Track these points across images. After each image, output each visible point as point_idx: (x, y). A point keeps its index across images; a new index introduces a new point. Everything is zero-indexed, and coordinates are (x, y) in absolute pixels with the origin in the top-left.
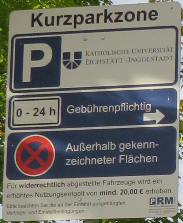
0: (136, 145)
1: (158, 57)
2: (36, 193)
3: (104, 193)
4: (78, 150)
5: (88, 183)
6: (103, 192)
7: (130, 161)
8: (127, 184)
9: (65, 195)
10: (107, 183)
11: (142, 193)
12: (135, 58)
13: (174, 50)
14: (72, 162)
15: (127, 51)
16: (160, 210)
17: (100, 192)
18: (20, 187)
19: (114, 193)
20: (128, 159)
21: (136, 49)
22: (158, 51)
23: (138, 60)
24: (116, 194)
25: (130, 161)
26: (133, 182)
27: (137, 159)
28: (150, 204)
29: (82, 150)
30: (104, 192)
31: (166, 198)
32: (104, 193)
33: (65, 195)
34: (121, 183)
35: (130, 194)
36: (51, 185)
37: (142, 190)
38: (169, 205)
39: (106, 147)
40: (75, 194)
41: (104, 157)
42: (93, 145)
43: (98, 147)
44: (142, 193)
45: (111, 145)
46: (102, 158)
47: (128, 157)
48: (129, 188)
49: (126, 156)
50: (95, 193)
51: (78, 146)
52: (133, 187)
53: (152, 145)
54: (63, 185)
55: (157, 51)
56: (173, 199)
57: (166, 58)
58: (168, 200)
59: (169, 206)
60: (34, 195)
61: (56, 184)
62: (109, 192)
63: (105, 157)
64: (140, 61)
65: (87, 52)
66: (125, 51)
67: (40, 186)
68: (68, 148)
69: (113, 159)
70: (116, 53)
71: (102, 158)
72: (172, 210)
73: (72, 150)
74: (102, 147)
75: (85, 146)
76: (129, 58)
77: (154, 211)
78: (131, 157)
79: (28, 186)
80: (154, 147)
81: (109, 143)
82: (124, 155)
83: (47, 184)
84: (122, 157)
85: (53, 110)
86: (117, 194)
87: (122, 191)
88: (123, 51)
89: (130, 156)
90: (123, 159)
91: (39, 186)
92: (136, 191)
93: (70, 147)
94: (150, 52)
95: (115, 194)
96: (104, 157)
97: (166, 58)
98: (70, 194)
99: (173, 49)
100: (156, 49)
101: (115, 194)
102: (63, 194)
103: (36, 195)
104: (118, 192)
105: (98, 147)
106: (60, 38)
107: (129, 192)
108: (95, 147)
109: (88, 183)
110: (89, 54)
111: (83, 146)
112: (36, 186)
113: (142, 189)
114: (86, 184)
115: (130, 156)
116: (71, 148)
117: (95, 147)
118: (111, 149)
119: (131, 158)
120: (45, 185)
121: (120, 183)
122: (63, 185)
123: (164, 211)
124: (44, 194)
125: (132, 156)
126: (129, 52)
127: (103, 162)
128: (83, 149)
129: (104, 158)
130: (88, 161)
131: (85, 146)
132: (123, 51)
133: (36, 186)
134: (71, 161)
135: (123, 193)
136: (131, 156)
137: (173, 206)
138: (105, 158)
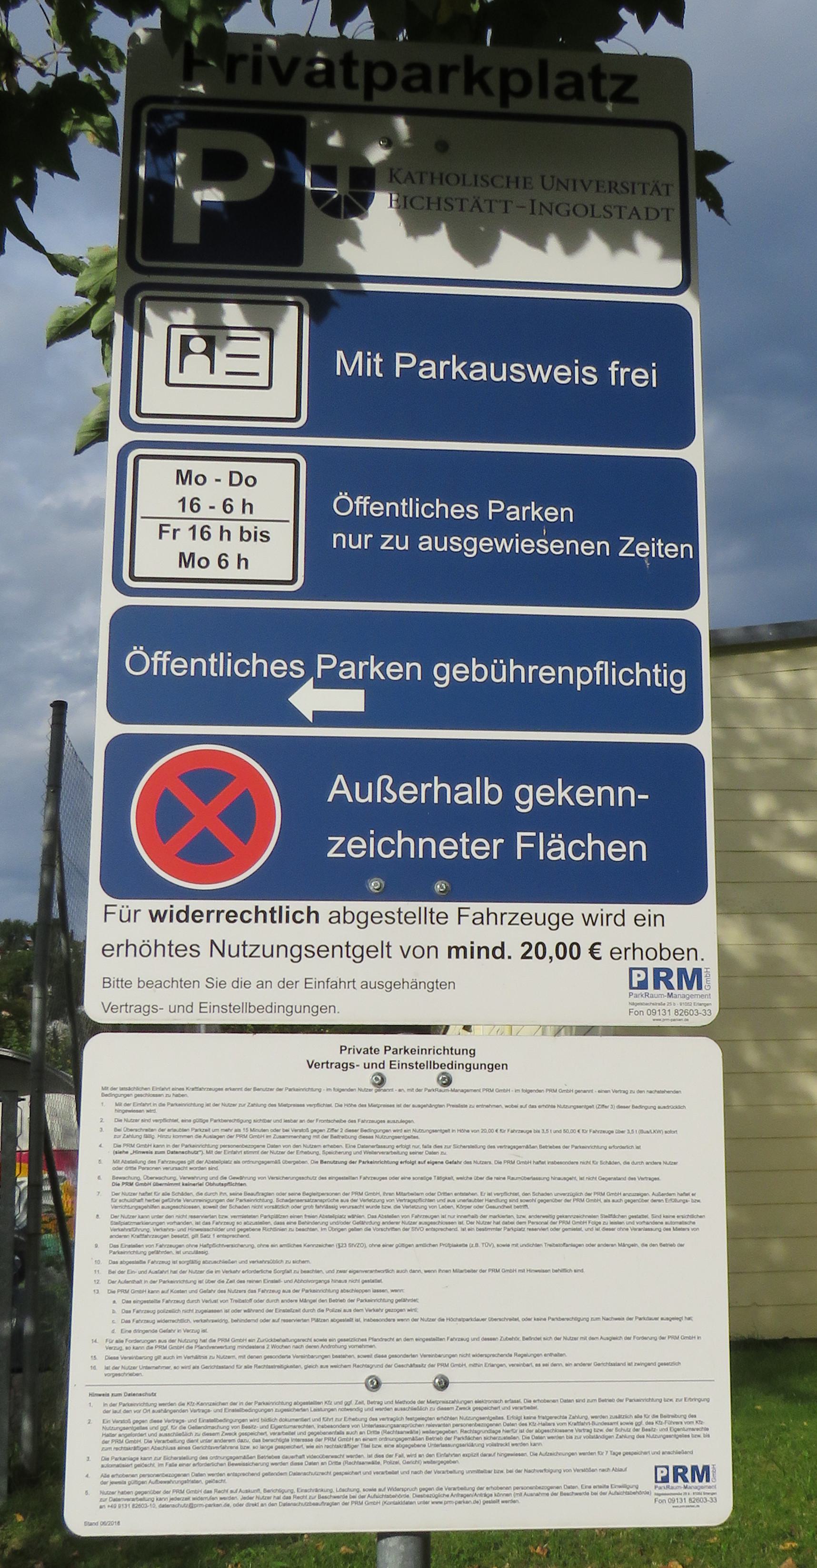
0: (572, 794)
1: (626, 207)
2: (212, 942)
3: (461, 951)
4: (369, 799)
5: (402, 916)
6: (457, 949)
7: (554, 854)
8: (544, 923)
9: (319, 952)
10: (472, 918)
11: (600, 958)
12: (551, 204)
13: (675, 191)
14: (350, 847)
15: (525, 179)
16: (663, 1007)
17: (450, 948)
18: (154, 920)
19: (498, 953)
20: (546, 848)
21: (553, 177)
22: (624, 191)
23: (561, 209)
24: (506, 956)
25: (554, 854)
26: (565, 920)
27: (577, 850)
28: (631, 987)
29: (385, 799)
30: (464, 948)
31: (695, 1468)
32: (461, 951)
33: (319, 952)
34: (522, 918)
35: (555, 957)
36: (269, 916)
37: (596, 947)
38: (701, 1484)
39: (469, 793)
40: (358, 952)
41: (464, 835)
42: (424, 787)
43: (442, 791)
44: (596, 955)
45: (487, 788)
46: (457, 838)
47: (547, 839)
48: (551, 939)
49: (538, 835)
50: (428, 951)
51: (370, 785)
52: (566, 935)
53: (626, 794)
54: (313, 916)
55: (619, 188)
56: (711, 1470)
57: (652, 214)
58: (686, 977)
59: (702, 1487)
60: (205, 949)
61: (288, 913)
62: (479, 949)
63: (467, 837)
64: (568, 214)
65: (391, 170)
66: (517, 178)
67: (227, 917)
68: (334, 791)
69: (496, 842)
70: (488, 183)
71: (457, 838)
72: (708, 1497)
73: (350, 800)
74: (453, 792)
75: (395, 788)
76: (533, 201)
77: (644, 1008)
78: (557, 839)
79: (182, 916)
80: (633, 804)
81: (478, 779)
82: (534, 834)
83: (253, 912)
84: (525, 840)
85: (314, 912)
86: (509, 957)
87: (527, 947)
88: (512, 179)
89: (553, 836)
90: (532, 845)
91: (223, 916)
92: (575, 947)
93: (340, 787)
94: (598, 190)
95: (502, 956)
96: (464, 835)
97: (652, 214)
98: (337, 950)
99: (670, 188)
100: (616, 184)
101: (502, 956)
102: (315, 950)
103: (214, 947)
104: (514, 949)
105: (442, 791)
106: (302, 123)
107: (551, 951)
108: (430, 791)
109: (402, 916)
110: (397, 176)
111: (388, 788)
112: (213, 916)
113: (599, 944)
114: (396, 916)
115: (553, 836)
116: (346, 791)
117: (430, 791)
118: (487, 801)
119: (558, 845)
120: (246, 917)
121: (518, 920)
122: (313, 916)
123: (676, 1011)
124: (244, 945)
125: (560, 836)
126: (530, 183)
127: (459, 851)
128: (390, 797)
129: (464, 840)
130: (406, 845)
131: (395, 788)
132: (512, 179)
133: (213, 916)
134: (345, 844)
135: (532, 953)
136: (557, 838)
137: (710, 1487)
138: (468, 840)
